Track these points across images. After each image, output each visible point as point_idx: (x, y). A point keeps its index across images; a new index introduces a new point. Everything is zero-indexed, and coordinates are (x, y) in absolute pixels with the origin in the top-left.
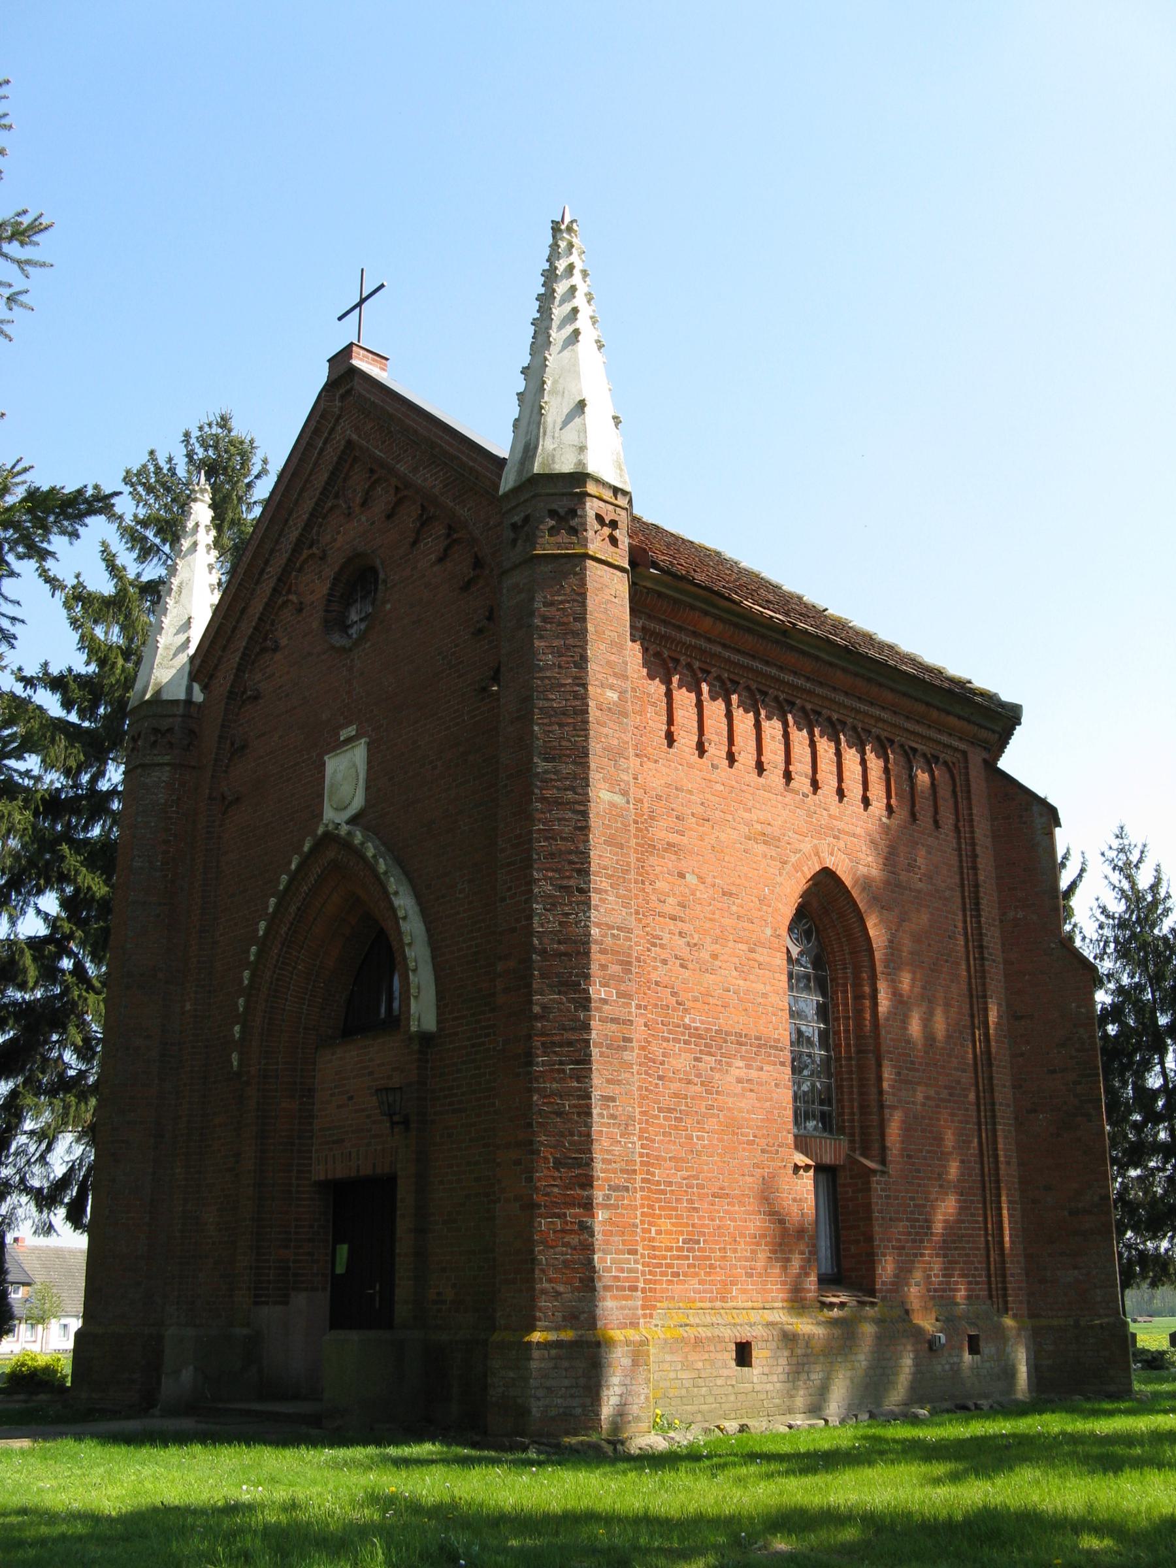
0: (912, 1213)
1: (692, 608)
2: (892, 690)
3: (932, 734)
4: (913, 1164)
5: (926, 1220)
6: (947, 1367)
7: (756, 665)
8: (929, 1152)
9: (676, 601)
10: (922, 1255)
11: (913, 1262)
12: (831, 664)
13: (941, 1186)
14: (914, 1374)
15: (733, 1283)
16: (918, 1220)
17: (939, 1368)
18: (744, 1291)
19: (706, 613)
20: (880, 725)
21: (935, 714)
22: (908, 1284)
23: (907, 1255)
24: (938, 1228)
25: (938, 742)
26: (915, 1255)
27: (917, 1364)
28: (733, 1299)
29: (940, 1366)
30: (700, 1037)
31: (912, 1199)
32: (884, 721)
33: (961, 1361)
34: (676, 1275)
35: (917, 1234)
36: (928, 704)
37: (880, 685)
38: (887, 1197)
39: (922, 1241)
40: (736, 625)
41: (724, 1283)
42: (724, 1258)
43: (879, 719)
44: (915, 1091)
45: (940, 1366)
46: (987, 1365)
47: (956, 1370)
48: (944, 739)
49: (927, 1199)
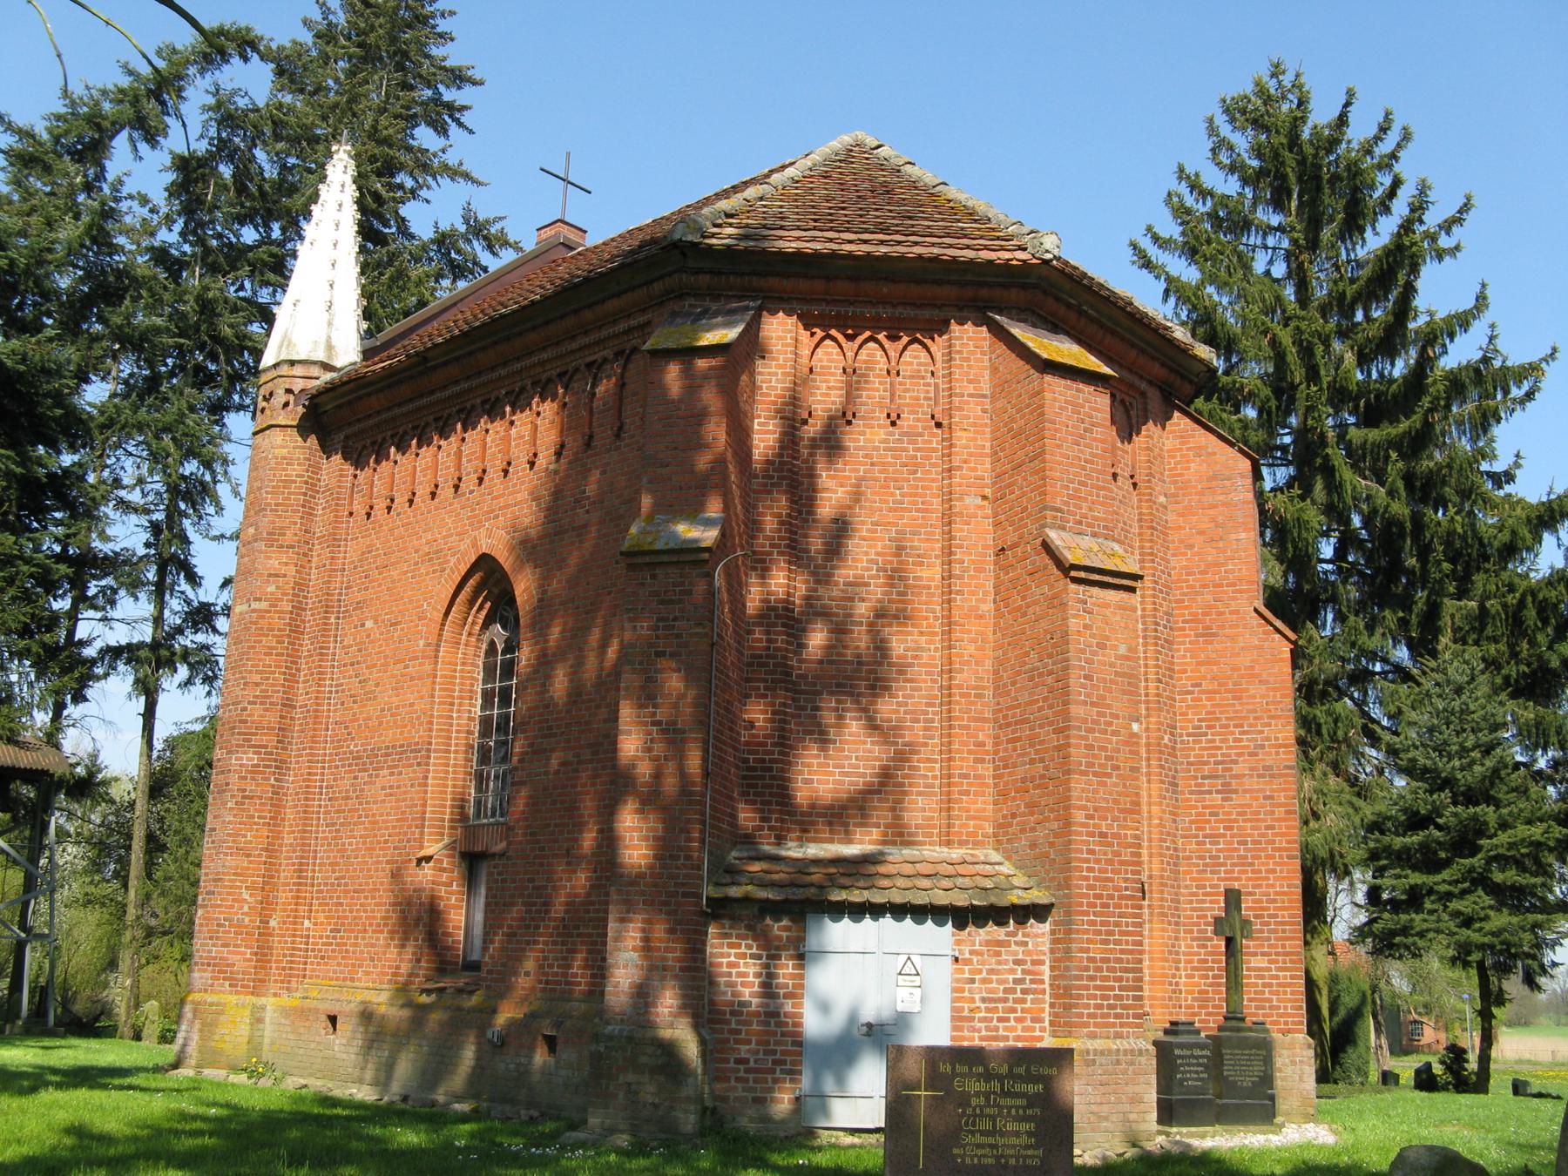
0: (530, 896)
1: (360, 398)
2: (534, 329)
3: (604, 333)
4: (538, 842)
5: (545, 904)
6: (512, 1067)
7: (425, 400)
8: (556, 825)
9: (349, 403)
10: (536, 943)
11: (524, 950)
12: (470, 354)
13: (568, 864)
14: (474, 1068)
15: (361, 966)
16: (535, 904)
17: (502, 1066)
18: (367, 973)
19: (369, 395)
20: (548, 366)
21: (588, 315)
22: (516, 974)
23: (518, 942)
24: (558, 909)
25: (616, 336)
26: (528, 943)
27: (478, 1059)
28: (359, 980)
29: (504, 1064)
30: (359, 758)
31: (532, 880)
32: (548, 360)
33: (530, 1062)
34: (323, 958)
35: (533, 919)
36: (576, 312)
37: (520, 334)
38: (504, 881)
39: (537, 927)
40: (389, 386)
41: (353, 965)
42: (356, 945)
43: (542, 363)
44: (548, 759)
45: (504, 1064)
46: (563, 1072)
47: (523, 1072)
48: (622, 326)
49: (549, 880)
